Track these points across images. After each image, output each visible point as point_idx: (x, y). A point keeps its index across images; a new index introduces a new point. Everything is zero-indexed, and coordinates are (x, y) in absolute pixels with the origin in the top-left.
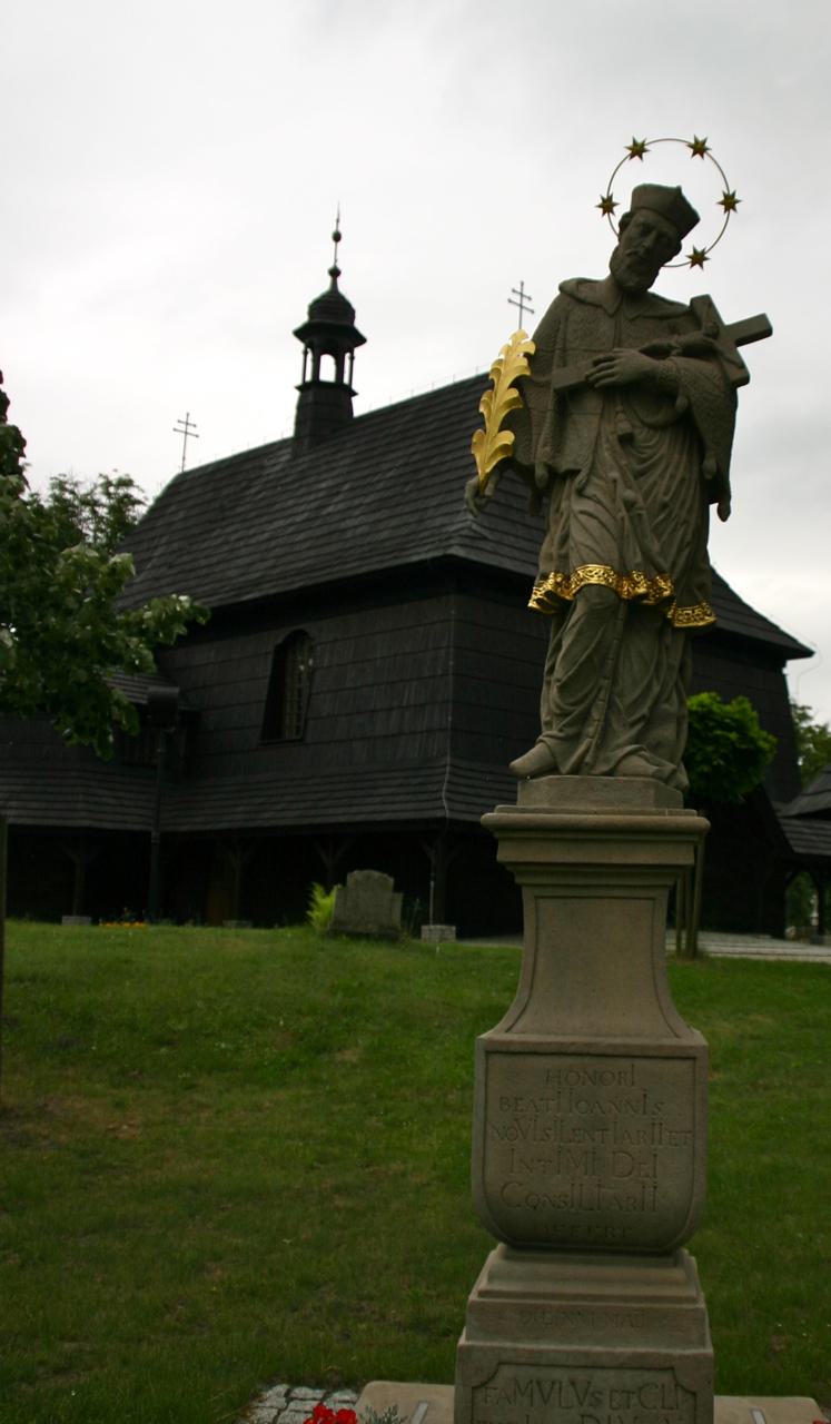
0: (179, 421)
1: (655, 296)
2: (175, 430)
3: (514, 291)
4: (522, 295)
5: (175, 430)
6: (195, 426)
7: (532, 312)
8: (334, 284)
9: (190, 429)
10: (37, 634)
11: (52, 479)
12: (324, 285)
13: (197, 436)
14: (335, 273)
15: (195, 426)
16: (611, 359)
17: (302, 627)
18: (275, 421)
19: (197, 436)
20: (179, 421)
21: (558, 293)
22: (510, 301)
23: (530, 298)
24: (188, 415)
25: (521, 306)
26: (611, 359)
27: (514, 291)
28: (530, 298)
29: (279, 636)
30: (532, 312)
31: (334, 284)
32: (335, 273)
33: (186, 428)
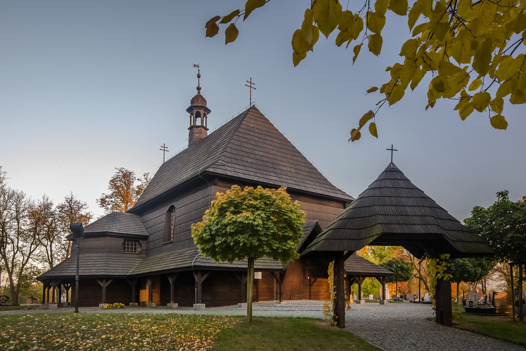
0: (161, 147)
1: (419, 15)
2: (160, 149)
3: (247, 81)
4: (251, 83)
5: (160, 149)
6: (167, 148)
7: (255, 89)
8: (199, 92)
9: (166, 149)
10: (219, 251)
11: (455, 109)
12: (196, 93)
13: (168, 151)
14: (199, 89)
15: (167, 148)
16: (430, 38)
17: (172, 204)
18: (183, 144)
19: (168, 151)
20: (161, 147)
21: (385, 15)
22: (246, 85)
23: (254, 84)
24: (164, 144)
25: (251, 87)
26: (430, 38)
27: (247, 81)
28: (254, 84)
29: (167, 208)
30: (255, 89)
31: (199, 92)
32: (199, 89)
33: (164, 148)
